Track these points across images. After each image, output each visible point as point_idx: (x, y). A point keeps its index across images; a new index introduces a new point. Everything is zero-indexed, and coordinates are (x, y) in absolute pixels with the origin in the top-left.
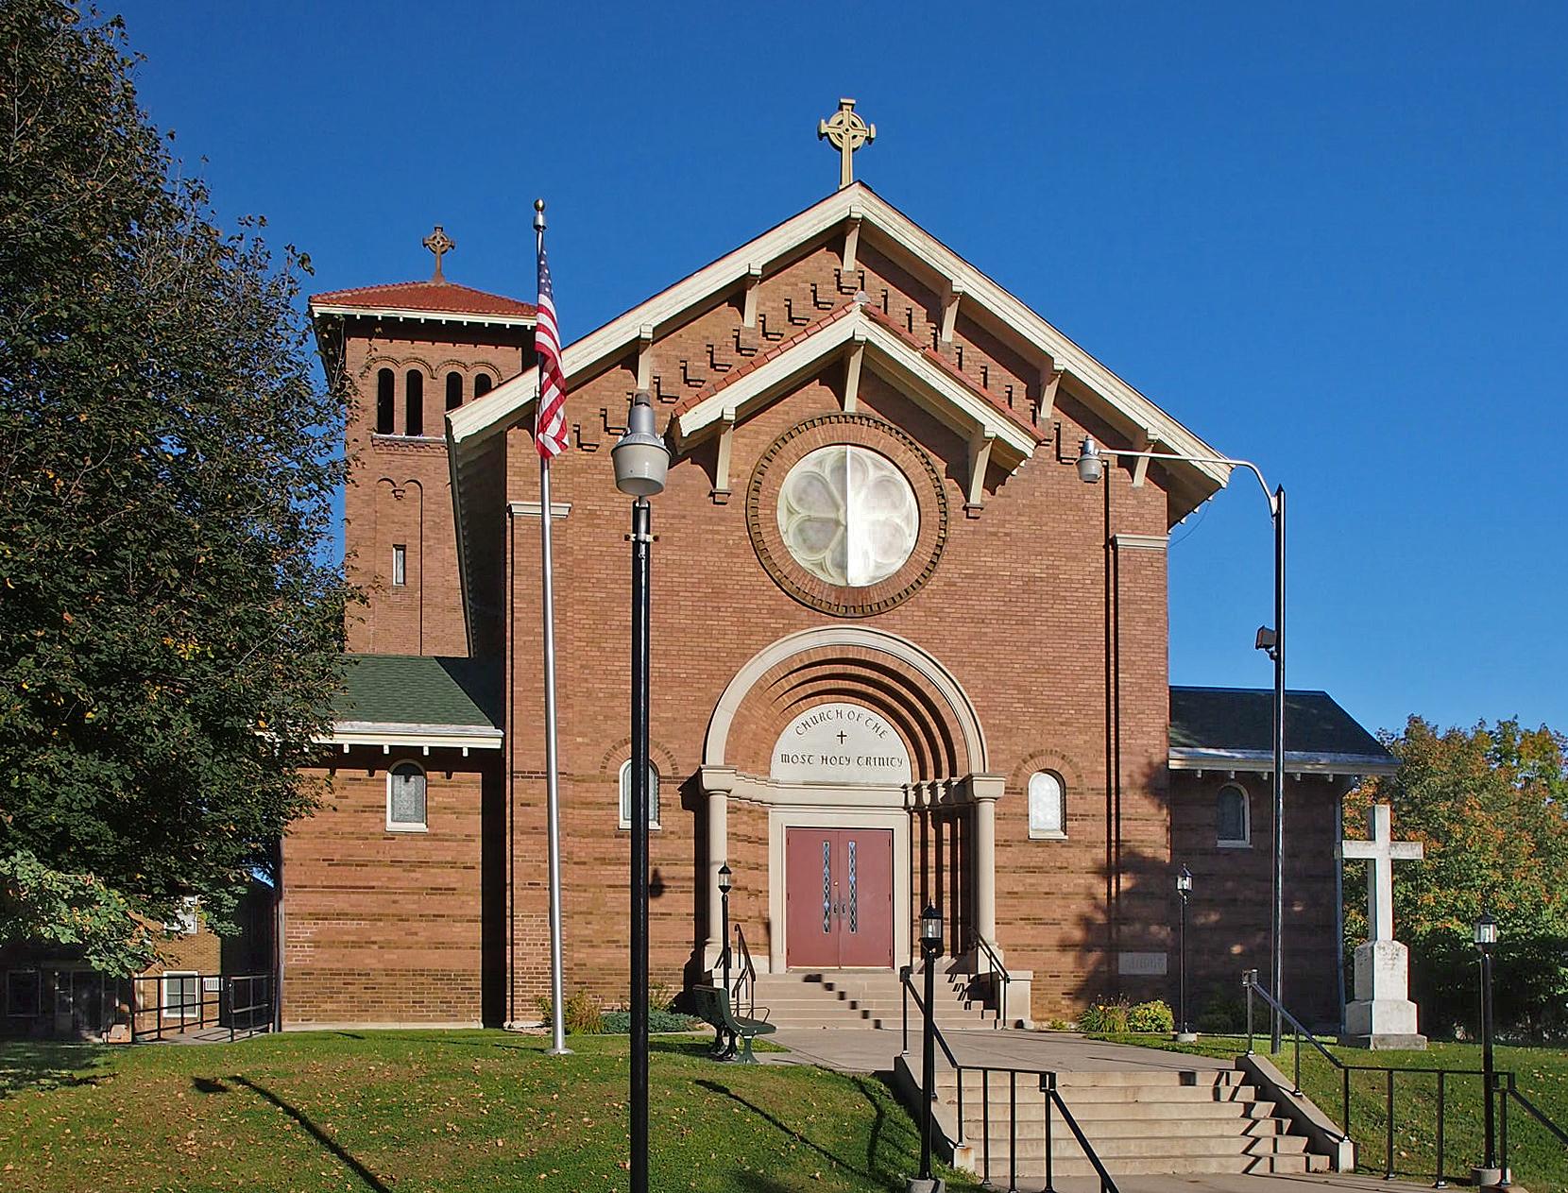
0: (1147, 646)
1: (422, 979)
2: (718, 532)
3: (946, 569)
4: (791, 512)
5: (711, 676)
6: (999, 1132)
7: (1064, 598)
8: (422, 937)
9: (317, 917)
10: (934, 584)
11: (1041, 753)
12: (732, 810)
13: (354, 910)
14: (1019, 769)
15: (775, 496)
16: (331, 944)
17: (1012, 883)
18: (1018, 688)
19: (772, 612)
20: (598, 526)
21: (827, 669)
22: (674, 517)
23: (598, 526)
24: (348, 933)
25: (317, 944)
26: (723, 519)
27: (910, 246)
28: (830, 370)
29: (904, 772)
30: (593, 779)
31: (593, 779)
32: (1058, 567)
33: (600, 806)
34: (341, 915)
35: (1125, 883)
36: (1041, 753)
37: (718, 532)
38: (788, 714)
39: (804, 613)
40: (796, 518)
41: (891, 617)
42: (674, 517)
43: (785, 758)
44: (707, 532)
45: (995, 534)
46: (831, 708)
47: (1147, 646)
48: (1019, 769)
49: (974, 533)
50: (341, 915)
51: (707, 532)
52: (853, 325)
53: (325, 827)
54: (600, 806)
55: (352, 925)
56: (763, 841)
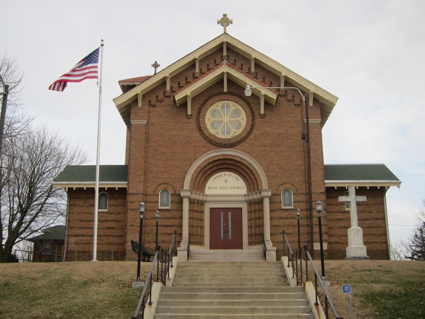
0: (316, 151)
1: (104, 254)
2: (188, 126)
3: (255, 132)
4: (209, 120)
5: (186, 165)
6: (299, 270)
7: (290, 139)
8: (105, 241)
9: (76, 236)
10: (251, 136)
11: (285, 183)
12: (190, 203)
13: (86, 234)
14: (278, 188)
15: (205, 115)
16: (80, 244)
17: (89, 231)
18: (277, 164)
19: (203, 147)
20: (155, 126)
21: (220, 162)
22: (176, 122)
23: (155, 126)
24: (85, 240)
25: (76, 244)
26: (190, 122)
27: (240, 48)
28: (219, 82)
29: (244, 191)
30: (151, 195)
31: (151, 195)
32: (288, 130)
33: (153, 202)
34: (83, 235)
35: (4, 247)
36: (285, 183)
37: (188, 126)
38: (210, 175)
39: (213, 147)
40: (210, 121)
41: (239, 147)
42: (176, 122)
43: (209, 188)
44: (185, 126)
45: (269, 122)
46: (223, 173)
47: (316, 151)
48: (278, 188)
49: (263, 122)
50: (83, 235)
51: (185, 126)
52: (224, 69)
53: (80, 211)
54: (153, 202)
55: (85, 238)
56: (202, 212)
